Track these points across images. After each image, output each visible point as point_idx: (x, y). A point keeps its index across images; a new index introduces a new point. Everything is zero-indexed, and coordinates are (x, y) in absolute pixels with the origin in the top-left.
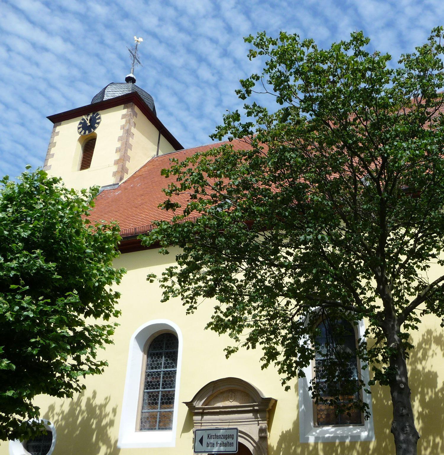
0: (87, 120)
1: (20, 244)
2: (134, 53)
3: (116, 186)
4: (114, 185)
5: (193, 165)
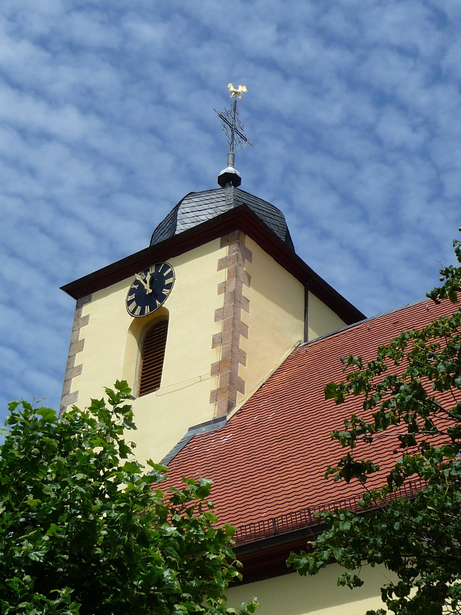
0: (146, 282)
1: (27, 578)
2: (230, 120)
3: (221, 424)
4: (215, 421)
5: (396, 364)
